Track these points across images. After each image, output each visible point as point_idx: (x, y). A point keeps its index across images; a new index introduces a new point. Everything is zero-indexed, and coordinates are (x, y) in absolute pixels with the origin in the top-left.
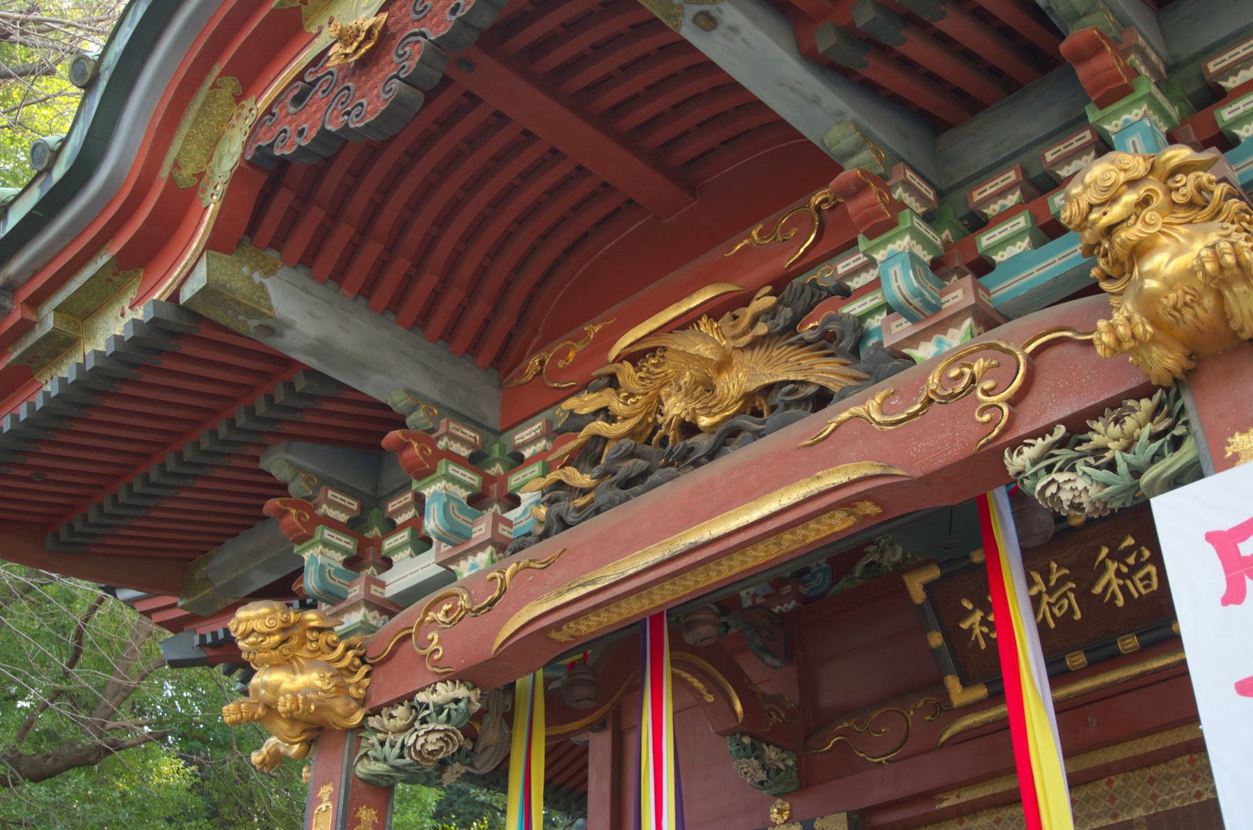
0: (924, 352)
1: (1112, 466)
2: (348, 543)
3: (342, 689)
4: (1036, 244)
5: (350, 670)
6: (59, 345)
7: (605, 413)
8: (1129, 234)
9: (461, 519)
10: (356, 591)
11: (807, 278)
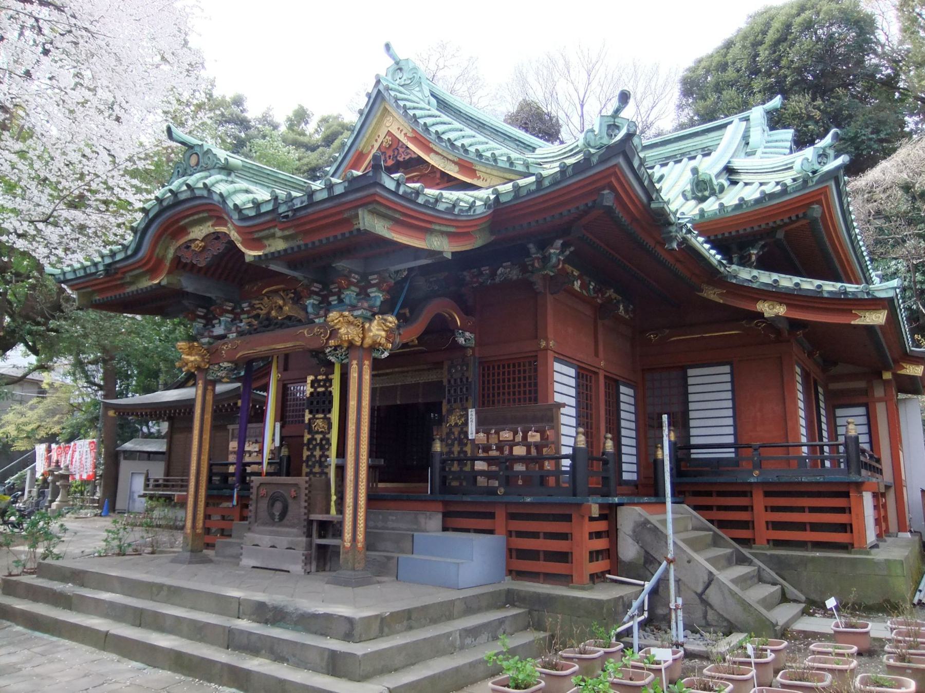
0: (317, 321)
2: (203, 321)
3: (203, 360)
5: (205, 355)
6: (131, 283)
8: (337, 327)
9: (229, 326)
10: (206, 334)
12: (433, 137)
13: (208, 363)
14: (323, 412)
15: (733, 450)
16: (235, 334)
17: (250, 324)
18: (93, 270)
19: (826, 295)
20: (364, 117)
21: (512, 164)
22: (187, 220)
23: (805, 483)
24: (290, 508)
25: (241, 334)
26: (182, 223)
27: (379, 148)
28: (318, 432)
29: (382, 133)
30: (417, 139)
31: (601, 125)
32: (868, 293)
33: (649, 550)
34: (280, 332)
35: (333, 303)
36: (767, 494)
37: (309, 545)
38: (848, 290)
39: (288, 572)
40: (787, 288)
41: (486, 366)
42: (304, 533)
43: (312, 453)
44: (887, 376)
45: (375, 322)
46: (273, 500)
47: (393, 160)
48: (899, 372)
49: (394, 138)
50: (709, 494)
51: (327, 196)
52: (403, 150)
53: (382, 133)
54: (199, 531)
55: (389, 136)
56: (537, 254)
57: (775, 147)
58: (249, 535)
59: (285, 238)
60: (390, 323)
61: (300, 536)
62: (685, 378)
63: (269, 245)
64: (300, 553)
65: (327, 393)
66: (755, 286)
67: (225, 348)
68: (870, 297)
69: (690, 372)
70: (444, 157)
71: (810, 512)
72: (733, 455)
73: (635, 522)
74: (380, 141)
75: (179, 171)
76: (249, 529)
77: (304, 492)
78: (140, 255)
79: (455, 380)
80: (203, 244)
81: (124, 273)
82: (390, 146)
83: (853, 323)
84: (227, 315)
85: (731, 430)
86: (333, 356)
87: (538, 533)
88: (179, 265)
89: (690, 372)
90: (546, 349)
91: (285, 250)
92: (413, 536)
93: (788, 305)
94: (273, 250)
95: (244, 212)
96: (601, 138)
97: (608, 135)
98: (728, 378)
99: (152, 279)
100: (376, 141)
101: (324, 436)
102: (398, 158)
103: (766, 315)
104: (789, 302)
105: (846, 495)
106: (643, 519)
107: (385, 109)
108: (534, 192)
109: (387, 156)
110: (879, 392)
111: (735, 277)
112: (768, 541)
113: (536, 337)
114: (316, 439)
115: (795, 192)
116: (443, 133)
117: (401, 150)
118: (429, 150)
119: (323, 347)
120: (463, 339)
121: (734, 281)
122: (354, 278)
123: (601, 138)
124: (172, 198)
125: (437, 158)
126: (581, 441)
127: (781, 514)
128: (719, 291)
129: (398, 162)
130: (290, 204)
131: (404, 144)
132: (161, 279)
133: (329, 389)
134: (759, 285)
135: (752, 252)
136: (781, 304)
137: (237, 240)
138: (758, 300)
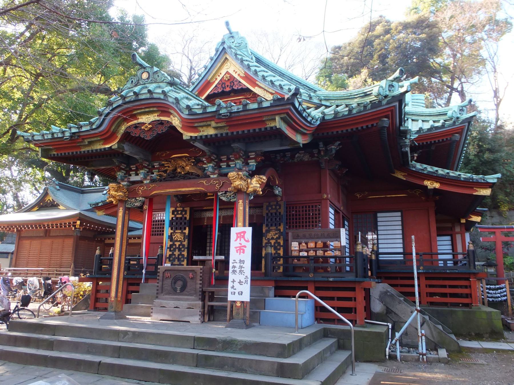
0: (212, 176)
1: (228, 198)
4: (227, 167)
5: (126, 192)
7: (169, 167)
11: (199, 158)
12: (260, 78)
13: (127, 197)
14: (181, 229)
15: (402, 256)
16: (148, 181)
17: (161, 176)
18: (60, 135)
19: (462, 179)
20: (213, 61)
21: (311, 98)
22: (139, 111)
23: (430, 273)
24: (188, 284)
25: (153, 181)
26: (135, 112)
27: (221, 80)
28: (177, 241)
29: (223, 72)
30: (247, 78)
31: (386, 84)
32: (484, 180)
33: (388, 306)
34: (182, 182)
35: (231, 166)
36: (426, 278)
37: (204, 307)
38: (474, 177)
39: (189, 322)
40: (442, 175)
41: (289, 206)
42: (199, 299)
43: (173, 253)
44: (463, 221)
45: (255, 179)
46: (175, 280)
47: (230, 88)
48: (469, 219)
49: (232, 77)
50: (396, 278)
51: (257, 107)
52: (237, 83)
53: (223, 72)
54: (119, 299)
55: (228, 74)
56: (323, 148)
57: (417, 103)
58: (156, 301)
59: (216, 128)
60: (264, 180)
61: (197, 301)
62: (376, 218)
63: (203, 131)
64: (198, 310)
65: (183, 218)
66: (425, 172)
67: (141, 190)
68: (485, 182)
69: (379, 215)
70: (265, 90)
71: (449, 288)
72: (402, 258)
73: (381, 291)
74: (221, 76)
75: (132, 81)
76: (157, 297)
77: (199, 275)
78: (101, 129)
79: (271, 214)
80: (151, 126)
81: (83, 139)
82: (229, 80)
83: (474, 194)
84: (146, 169)
85: (401, 245)
86: (224, 197)
87: (334, 297)
88: (127, 137)
89: (379, 215)
90: (327, 199)
91: (216, 135)
92: (265, 299)
93: (441, 183)
94: (205, 134)
95: (193, 110)
96: (386, 91)
97: (389, 90)
98: (400, 218)
99: (105, 144)
100: (219, 76)
101: (181, 243)
102: (234, 87)
103: (429, 187)
104: (441, 181)
105: (467, 279)
106: (385, 290)
107: (226, 59)
108: (346, 115)
109: (226, 85)
110: (458, 229)
111: (415, 167)
112: (427, 302)
113: (320, 192)
114: (175, 245)
115: (449, 127)
116: (267, 77)
117: (235, 83)
118: (255, 84)
119: (217, 192)
120: (277, 191)
121: (414, 169)
122: (242, 153)
123: (386, 91)
124: (134, 97)
125: (260, 90)
126: (360, 248)
127: (434, 288)
128: (403, 174)
129: (233, 89)
130: (229, 109)
131: (238, 80)
132: (114, 144)
133: (173, 216)
134: (427, 172)
135: (415, 155)
136: (437, 182)
137: (177, 126)
138: (425, 179)
